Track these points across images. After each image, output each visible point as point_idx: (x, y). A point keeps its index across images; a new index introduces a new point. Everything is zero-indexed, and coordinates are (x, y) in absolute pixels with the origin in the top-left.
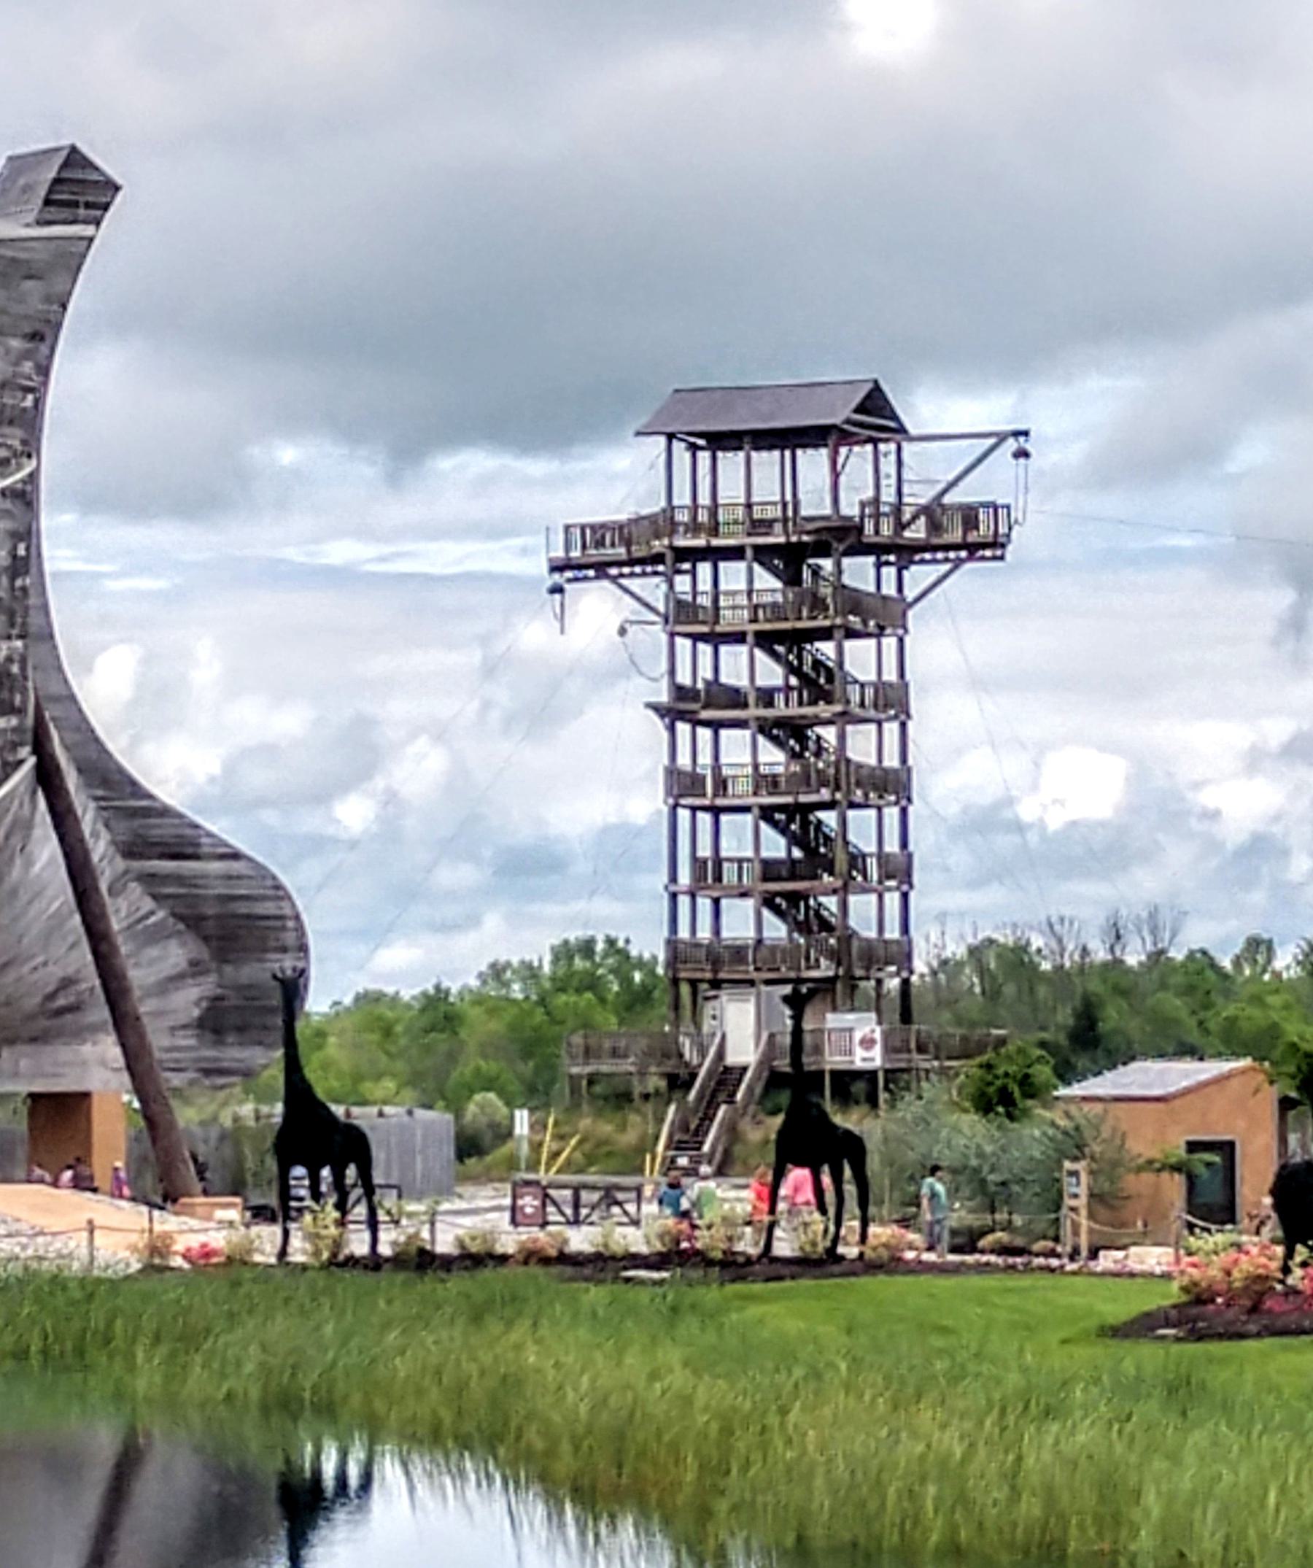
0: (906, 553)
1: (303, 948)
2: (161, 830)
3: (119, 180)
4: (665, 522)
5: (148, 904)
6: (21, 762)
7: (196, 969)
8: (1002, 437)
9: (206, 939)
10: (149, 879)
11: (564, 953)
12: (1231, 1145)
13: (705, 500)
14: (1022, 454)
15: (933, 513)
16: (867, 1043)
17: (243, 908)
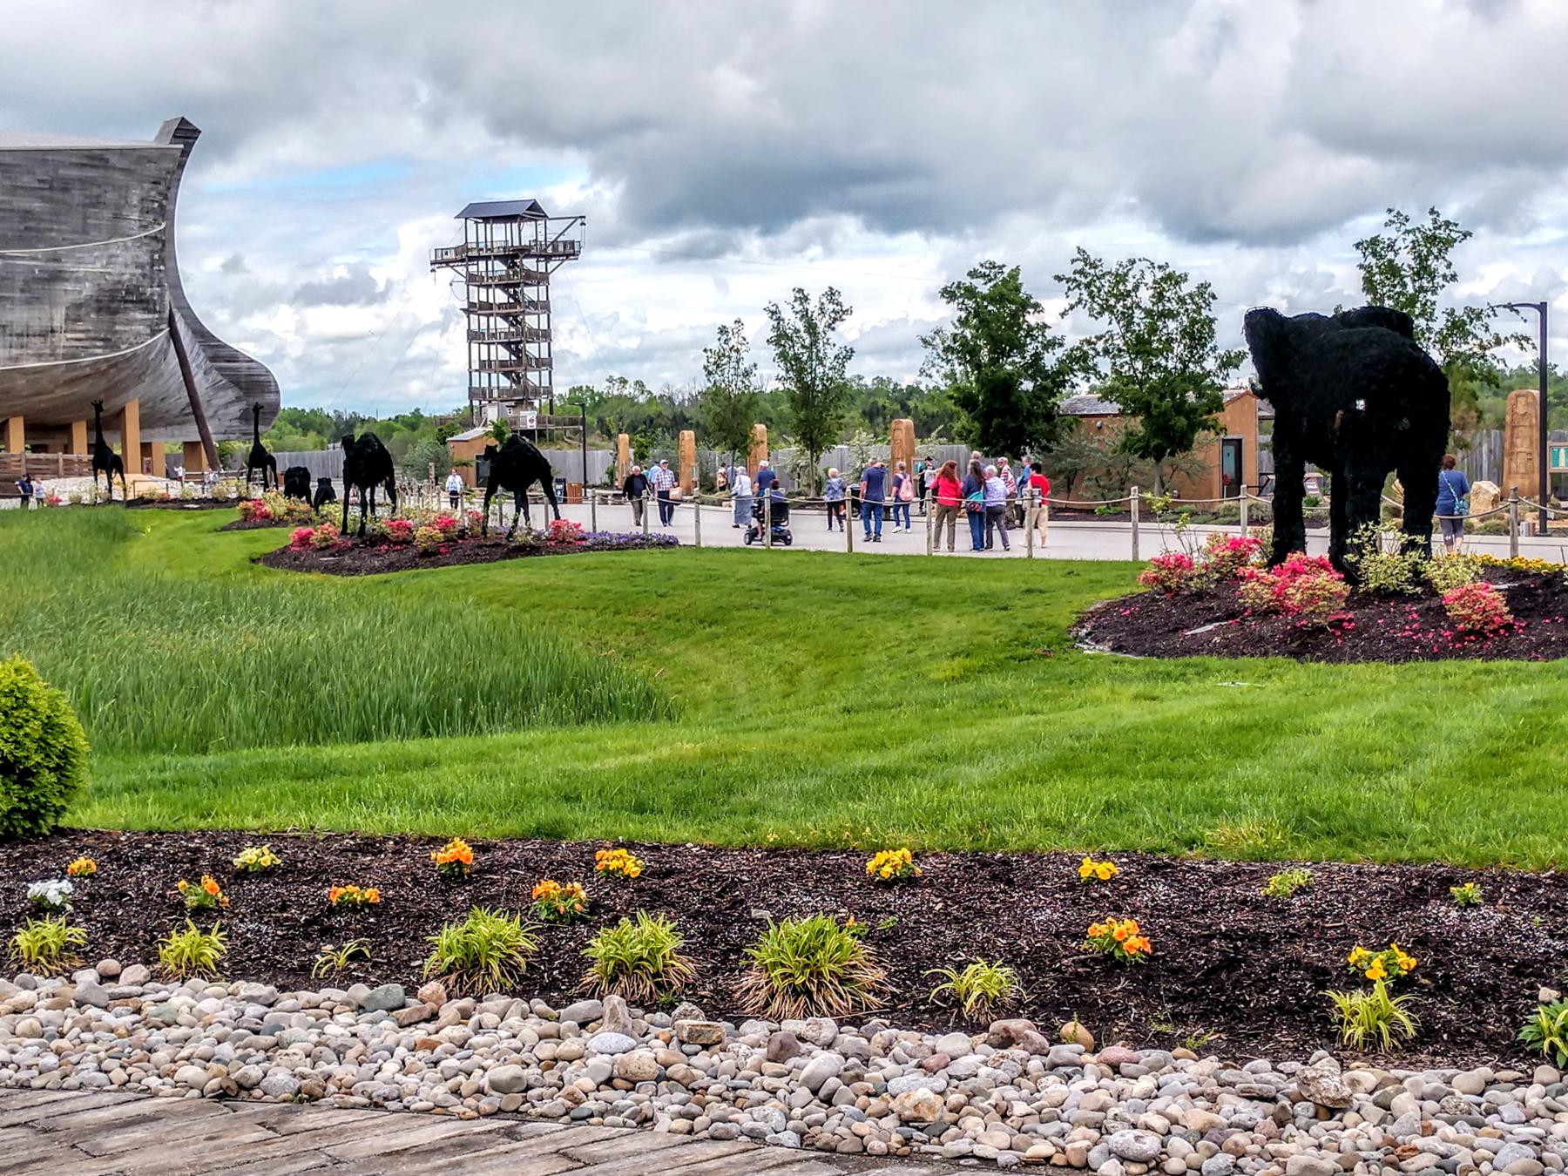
0: (548, 258)
1: (278, 392)
2: (223, 353)
3: (199, 128)
4: (465, 248)
5: (220, 378)
6: (161, 330)
7: (238, 399)
8: (576, 218)
9: (241, 388)
10: (217, 369)
11: (572, 390)
12: (1239, 441)
13: (489, 239)
14: (583, 224)
15: (554, 243)
16: (531, 421)
17: (255, 378)
